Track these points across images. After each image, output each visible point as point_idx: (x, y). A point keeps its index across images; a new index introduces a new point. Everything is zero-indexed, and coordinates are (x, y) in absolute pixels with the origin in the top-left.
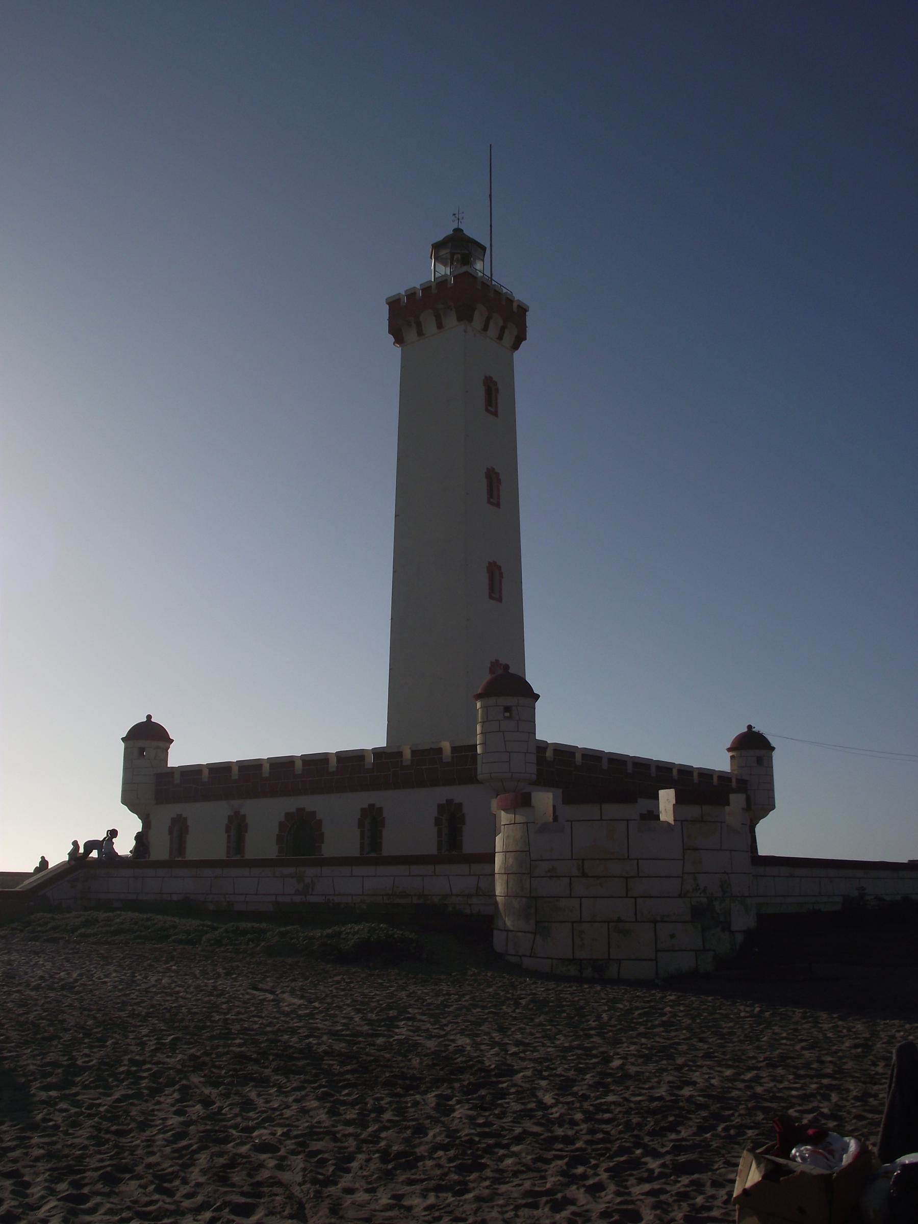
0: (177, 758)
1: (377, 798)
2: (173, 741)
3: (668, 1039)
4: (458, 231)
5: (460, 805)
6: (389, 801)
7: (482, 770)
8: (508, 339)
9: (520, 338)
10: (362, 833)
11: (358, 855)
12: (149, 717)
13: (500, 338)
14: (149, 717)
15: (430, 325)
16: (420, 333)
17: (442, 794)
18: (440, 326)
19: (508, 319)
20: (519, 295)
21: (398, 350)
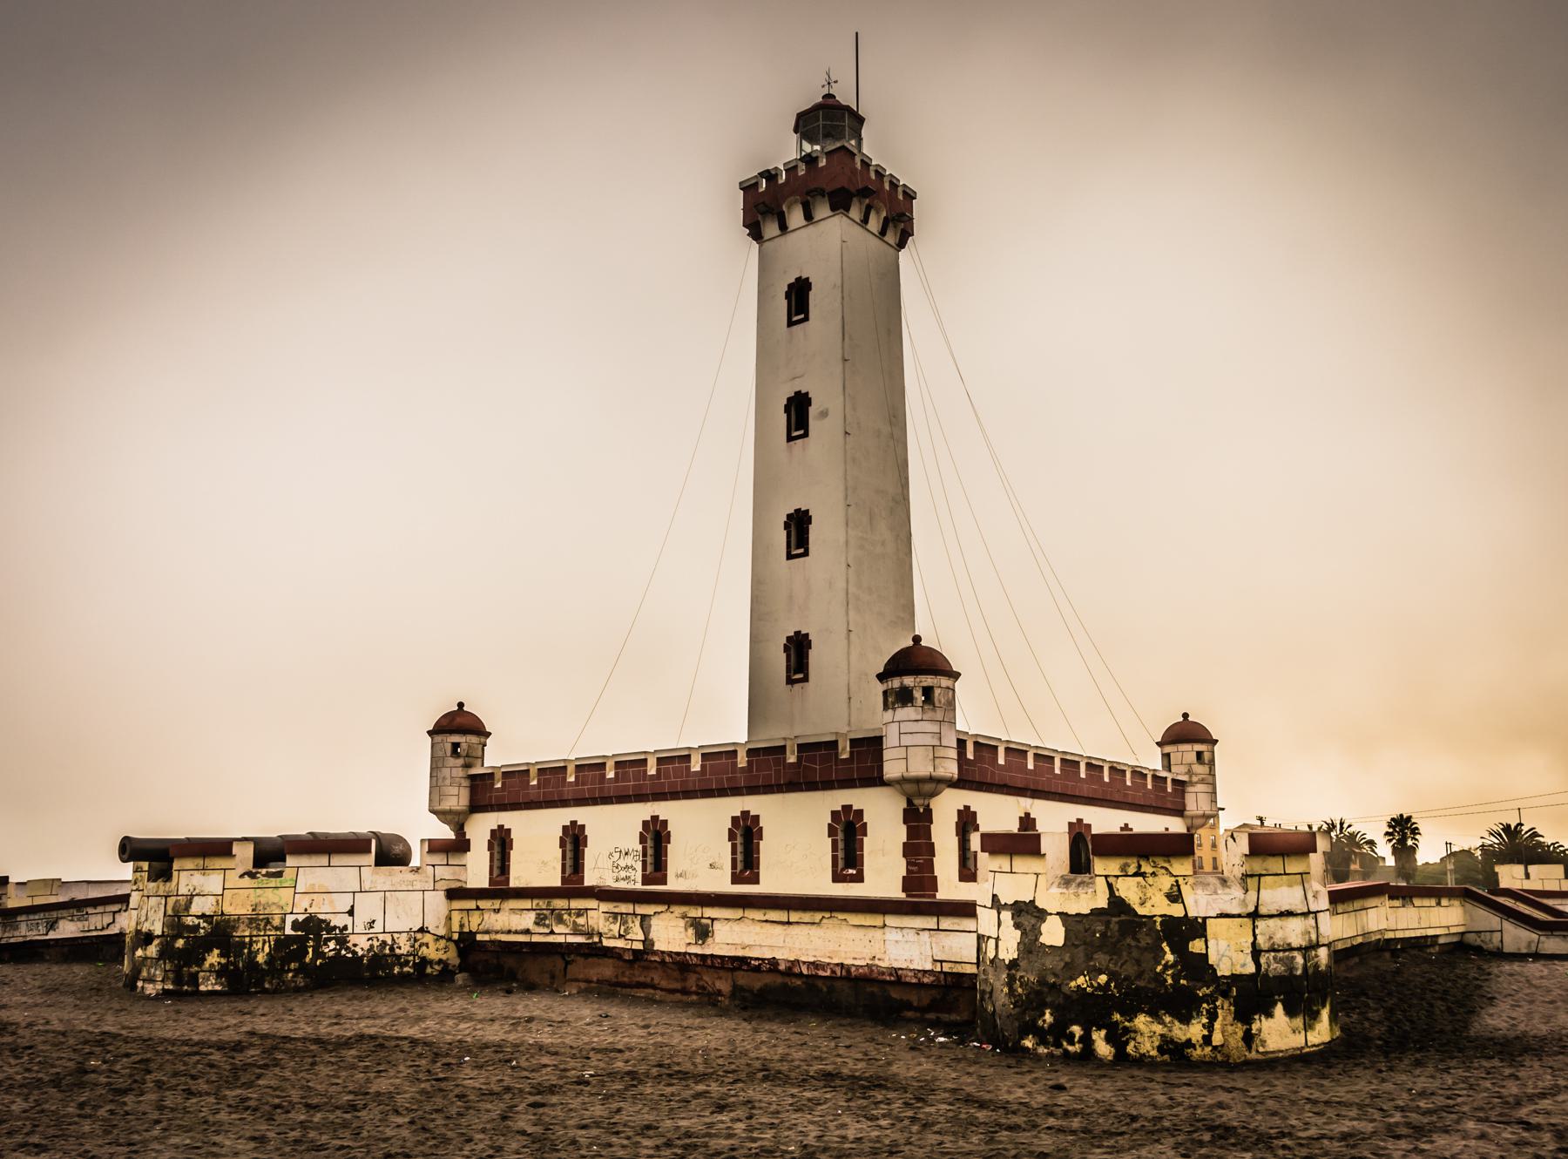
1: (663, 809)
2: (489, 734)
3: (1448, 1098)
4: (829, 96)
5: (665, 822)
6: (516, 822)
7: (892, 770)
8: (891, 237)
10: (835, 844)
11: (559, 884)
13: (865, 221)
15: (796, 218)
16: (783, 227)
18: (809, 217)
19: (891, 211)
21: (755, 245)
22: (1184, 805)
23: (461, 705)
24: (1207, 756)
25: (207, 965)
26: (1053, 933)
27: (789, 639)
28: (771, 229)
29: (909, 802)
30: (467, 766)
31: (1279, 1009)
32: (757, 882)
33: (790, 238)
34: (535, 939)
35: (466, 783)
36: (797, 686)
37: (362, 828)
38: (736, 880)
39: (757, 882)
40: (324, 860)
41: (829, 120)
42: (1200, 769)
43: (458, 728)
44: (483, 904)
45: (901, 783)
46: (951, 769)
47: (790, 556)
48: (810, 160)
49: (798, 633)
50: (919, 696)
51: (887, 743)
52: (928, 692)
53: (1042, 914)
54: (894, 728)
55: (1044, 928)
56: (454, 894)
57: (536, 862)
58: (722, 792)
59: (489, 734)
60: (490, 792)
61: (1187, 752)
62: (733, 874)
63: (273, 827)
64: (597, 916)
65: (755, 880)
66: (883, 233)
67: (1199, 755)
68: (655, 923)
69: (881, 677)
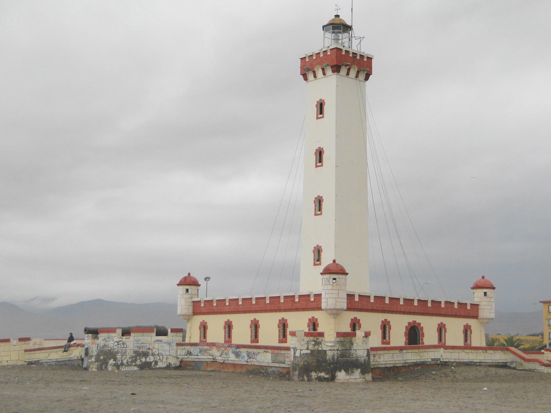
5: (317, 319)
7: (323, 306)
8: (362, 76)
13: (348, 74)
15: (319, 73)
17: (280, 315)
18: (324, 74)
23: (189, 274)
25: (109, 364)
27: (315, 247)
28: (310, 76)
31: (343, 371)
32: (286, 342)
35: (192, 304)
37: (152, 324)
38: (280, 341)
39: (286, 342)
40: (141, 334)
45: (326, 310)
51: (323, 296)
57: (216, 334)
60: (198, 308)
62: (279, 340)
63: (126, 325)
64: (215, 352)
65: (258, 342)
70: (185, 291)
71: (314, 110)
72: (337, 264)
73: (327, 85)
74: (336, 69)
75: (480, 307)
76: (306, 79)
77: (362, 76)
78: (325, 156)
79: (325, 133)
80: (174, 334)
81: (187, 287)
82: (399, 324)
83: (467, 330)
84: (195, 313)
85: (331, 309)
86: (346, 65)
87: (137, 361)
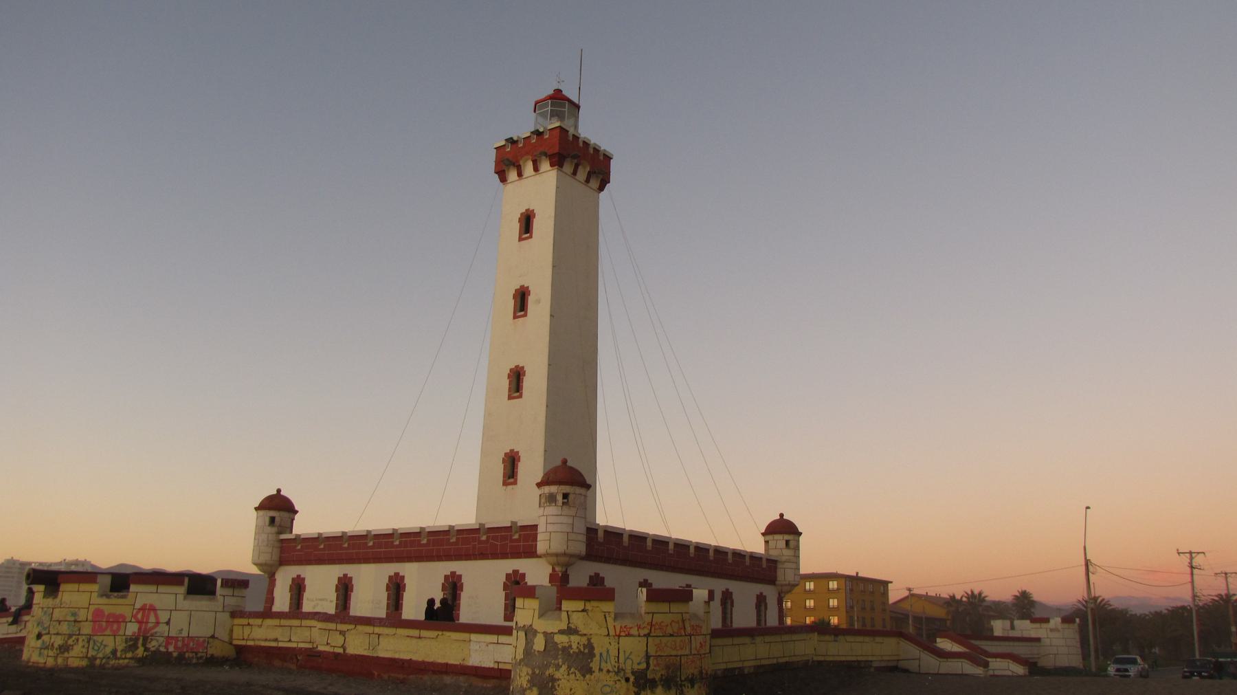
0: (304, 526)
4: (558, 91)
5: (460, 577)
7: (541, 547)
8: (595, 184)
9: (604, 183)
12: (279, 491)
13: (575, 173)
14: (279, 491)
15: (528, 168)
16: (520, 175)
17: (391, 568)
18: (536, 169)
20: (604, 146)
22: (776, 577)
24: (792, 544)
26: (539, 644)
28: (512, 175)
29: (553, 569)
30: (280, 533)
33: (524, 182)
34: (281, 645)
36: (510, 487)
40: (153, 588)
41: (560, 103)
42: (788, 553)
43: (278, 507)
44: (251, 621)
45: (547, 555)
46: (581, 548)
47: (510, 398)
48: (538, 133)
49: (512, 451)
50: (560, 498)
51: (540, 529)
52: (565, 496)
53: (535, 632)
54: (543, 520)
55: (536, 640)
56: (234, 615)
58: (439, 558)
59: (296, 512)
61: (779, 540)
66: (587, 181)
67: (787, 542)
68: (350, 637)
69: (539, 485)
70: (267, 520)
71: (516, 227)
72: (571, 469)
73: (540, 188)
74: (557, 161)
75: (779, 566)
76: (503, 179)
77: (595, 184)
78: (531, 300)
79: (535, 264)
80: (229, 591)
81: (272, 513)
82: (370, 586)
83: (761, 600)
84: (283, 562)
85: (557, 555)
86: (574, 157)
87: (137, 648)
